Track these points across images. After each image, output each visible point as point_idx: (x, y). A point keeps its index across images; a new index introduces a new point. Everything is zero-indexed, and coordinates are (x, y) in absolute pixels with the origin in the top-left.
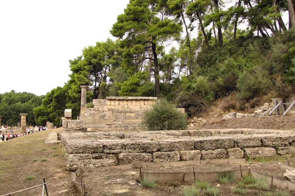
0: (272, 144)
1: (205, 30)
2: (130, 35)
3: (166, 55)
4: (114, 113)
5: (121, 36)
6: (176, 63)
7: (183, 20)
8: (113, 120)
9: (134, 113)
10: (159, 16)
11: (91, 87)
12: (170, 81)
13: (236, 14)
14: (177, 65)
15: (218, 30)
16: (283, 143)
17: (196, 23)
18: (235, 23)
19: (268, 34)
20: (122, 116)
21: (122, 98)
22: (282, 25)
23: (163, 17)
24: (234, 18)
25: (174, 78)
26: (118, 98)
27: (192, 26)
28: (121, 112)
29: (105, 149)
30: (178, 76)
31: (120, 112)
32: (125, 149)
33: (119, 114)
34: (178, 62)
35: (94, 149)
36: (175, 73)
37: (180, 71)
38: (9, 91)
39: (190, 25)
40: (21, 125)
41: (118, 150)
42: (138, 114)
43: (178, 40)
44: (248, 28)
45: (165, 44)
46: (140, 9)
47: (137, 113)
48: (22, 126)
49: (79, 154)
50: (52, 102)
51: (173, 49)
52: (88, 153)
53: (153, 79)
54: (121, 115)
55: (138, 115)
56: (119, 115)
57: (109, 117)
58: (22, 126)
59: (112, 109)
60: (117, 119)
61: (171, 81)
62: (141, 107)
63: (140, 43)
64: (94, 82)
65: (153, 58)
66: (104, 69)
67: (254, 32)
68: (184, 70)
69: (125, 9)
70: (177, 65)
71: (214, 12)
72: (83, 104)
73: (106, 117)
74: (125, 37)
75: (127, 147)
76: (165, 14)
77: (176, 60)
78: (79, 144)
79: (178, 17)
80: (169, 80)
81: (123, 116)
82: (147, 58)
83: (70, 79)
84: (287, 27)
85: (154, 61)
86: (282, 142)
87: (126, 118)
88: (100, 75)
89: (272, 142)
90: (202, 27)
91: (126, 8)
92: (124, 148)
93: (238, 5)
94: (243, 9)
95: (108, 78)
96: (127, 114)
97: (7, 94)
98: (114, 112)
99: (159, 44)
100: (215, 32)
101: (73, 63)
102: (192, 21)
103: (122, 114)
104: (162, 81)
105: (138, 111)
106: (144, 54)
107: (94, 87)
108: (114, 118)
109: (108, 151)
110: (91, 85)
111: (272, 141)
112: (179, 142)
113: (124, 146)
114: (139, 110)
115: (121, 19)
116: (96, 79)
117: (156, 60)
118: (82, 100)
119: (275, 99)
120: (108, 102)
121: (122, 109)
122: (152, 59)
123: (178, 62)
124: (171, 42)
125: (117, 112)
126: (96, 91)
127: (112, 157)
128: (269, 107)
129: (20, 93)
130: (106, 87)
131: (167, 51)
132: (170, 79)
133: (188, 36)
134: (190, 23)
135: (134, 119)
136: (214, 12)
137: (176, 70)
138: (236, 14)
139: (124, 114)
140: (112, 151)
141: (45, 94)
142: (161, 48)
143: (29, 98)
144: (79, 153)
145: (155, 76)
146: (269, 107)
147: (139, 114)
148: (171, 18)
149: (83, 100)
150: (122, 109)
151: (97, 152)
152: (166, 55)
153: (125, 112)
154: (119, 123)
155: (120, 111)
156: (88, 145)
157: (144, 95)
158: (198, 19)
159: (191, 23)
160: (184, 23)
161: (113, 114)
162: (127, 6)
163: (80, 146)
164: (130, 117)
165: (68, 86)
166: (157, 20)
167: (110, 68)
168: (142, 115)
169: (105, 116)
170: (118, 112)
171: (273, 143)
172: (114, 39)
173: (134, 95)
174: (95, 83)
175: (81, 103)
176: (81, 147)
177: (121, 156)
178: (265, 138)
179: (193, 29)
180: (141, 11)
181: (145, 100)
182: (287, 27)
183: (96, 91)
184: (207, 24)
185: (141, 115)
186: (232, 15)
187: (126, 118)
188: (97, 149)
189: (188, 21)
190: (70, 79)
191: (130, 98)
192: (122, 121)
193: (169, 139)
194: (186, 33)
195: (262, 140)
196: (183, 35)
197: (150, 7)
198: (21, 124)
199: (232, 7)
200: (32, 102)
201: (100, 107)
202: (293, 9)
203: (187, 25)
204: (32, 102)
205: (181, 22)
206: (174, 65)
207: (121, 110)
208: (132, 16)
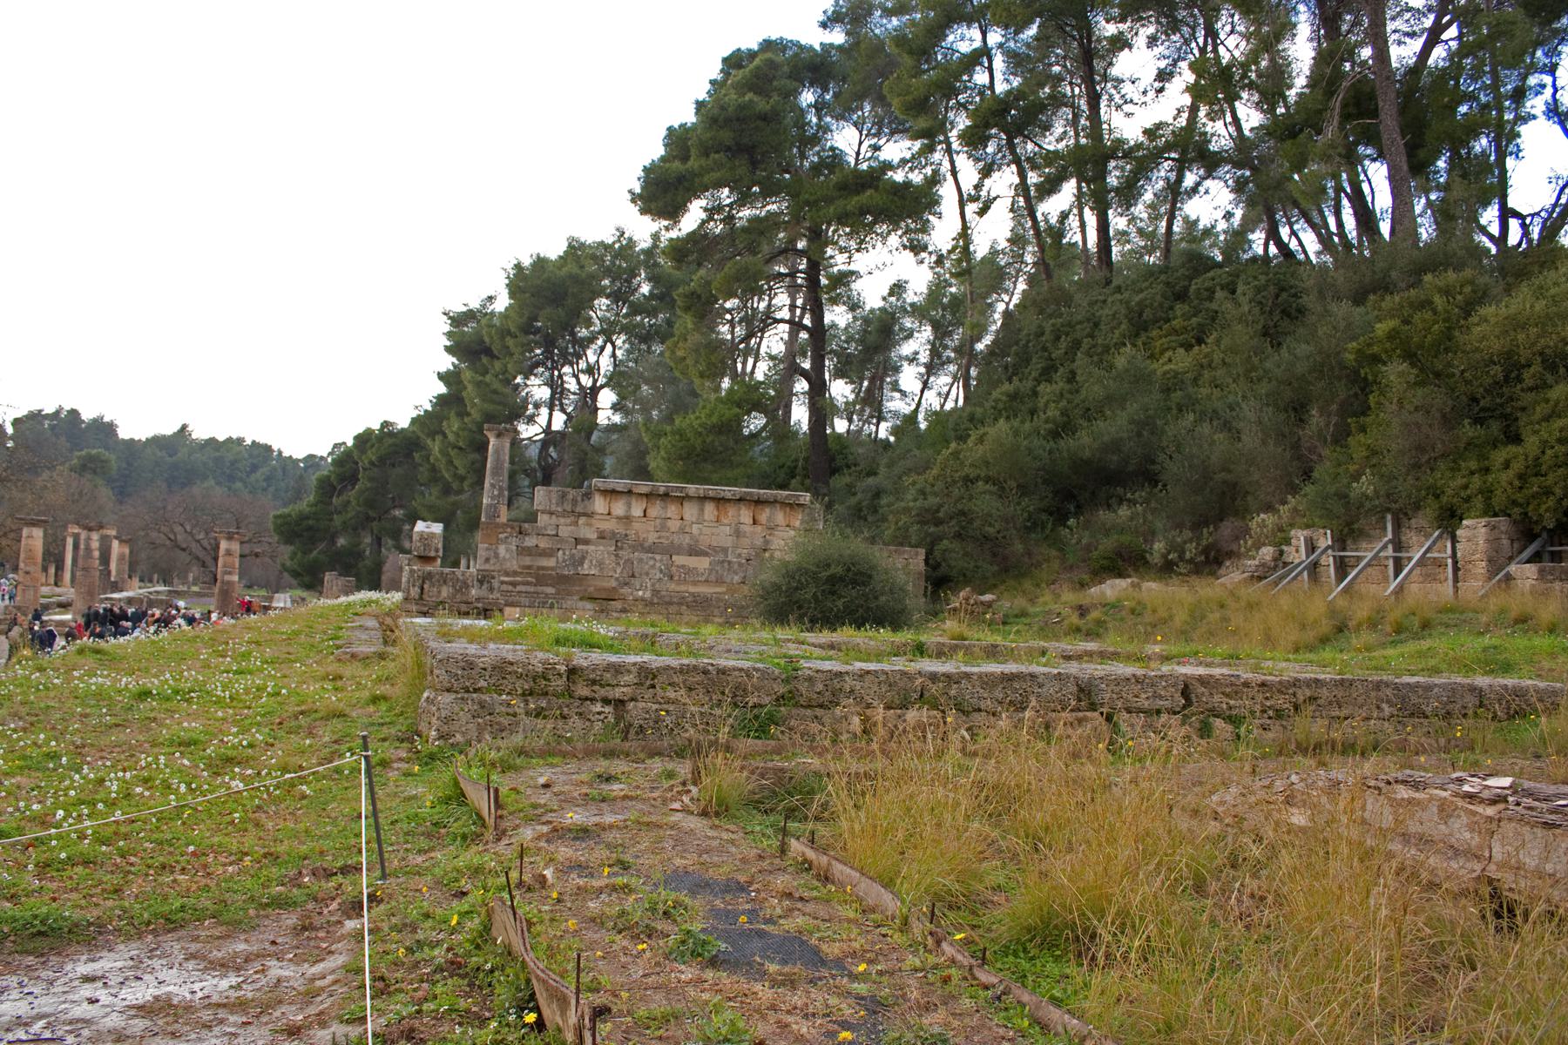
0: (1225, 706)
1: (1040, 217)
2: (711, 212)
3: (868, 308)
4: (621, 552)
5: (673, 212)
6: (907, 349)
7: (946, 165)
8: (617, 579)
9: (706, 554)
10: (846, 139)
11: (527, 431)
12: (877, 425)
13: (1173, 155)
14: (912, 359)
15: (1094, 218)
16: (1268, 704)
17: (1004, 182)
18: (1175, 193)
19: (1304, 251)
20: (653, 567)
21: (661, 487)
22: (1366, 218)
23: (860, 143)
24: (1165, 169)
25: (896, 414)
26: (643, 487)
27: (983, 193)
28: (652, 549)
29: (574, 682)
30: (913, 407)
31: (650, 550)
32: (653, 686)
33: (644, 556)
34: (919, 342)
35: (534, 680)
36: (904, 394)
37: (925, 386)
38: (169, 429)
39: (978, 187)
40: (216, 580)
41: (625, 690)
42: (723, 562)
43: (917, 248)
44: (1228, 216)
45: (861, 262)
46: (762, 105)
47: (721, 557)
48: (223, 582)
49: (475, 695)
50: (355, 484)
51: (898, 288)
52: (509, 694)
53: (800, 414)
54: (651, 563)
55: (726, 564)
56: (641, 560)
57: (600, 564)
58: (223, 582)
59: (614, 534)
60: (633, 576)
61: (884, 426)
62: (738, 533)
63: (833, 149)
64: (544, 411)
65: (807, 321)
66: (591, 356)
67: (1251, 237)
68: (942, 381)
69: (701, 99)
70: (912, 359)
71: (1083, 141)
72: (490, 506)
73: (586, 566)
74: (693, 216)
75: (661, 680)
76: (869, 131)
77: (910, 336)
78: (479, 657)
79: (930, 149)
80: (875, 421)
81: (658, 565)
82: (782, 321)
83: (441, 389)
84: (1385, 228)
85: (811, 335)
86: (1267, 698)
87: (671, 577)
88: (573, 380)
89: (1225, 700)
90: (1028, 199)
91: (702, 96)
92: (649, 682)
93: (1185, 115)
94: (1205, 139)
95: (607, 398)
96: (679, 560)
97: (156, 441)
98: (622, 548)
99: (840, 262)
100: (1083, 226)
101: (458, 320)
102: (986, 172)
103: (658, 557)
104: (841, 426)
105: (725, 550)
106: (771, 300)
107: (544, 431)
108: (619, 571)
109: (585, 692)
110: (531, 420)
111: (1227, 695)
112: (864, 674)
113: (647, 676)
114: (728, 542)
115: (677, 139)
116: (552, 397)
117: (819, 332)
118: (487, 485)
119: (1305, 532)
120: (599, 504)
121: (656, 535)
122: (805, 328)
123: (919, 342)
124: (888, 258)
125: (634, 549)
126: (551, 449)
127: (599, 713)
128: (1276, 566)
129: (212, 441)
130: (594, 437)
131: (872, 293)
132: (880, 419)
133: (965, 234)
134: (975, 181)
135: (707, 581)
136: (1083, 141)
137: (909, 378)
138: (1173, 155)
139: (666, 557)
140: (602, 692)
141: (323, 449)
142: (844, 278)
143: (255, 461)
144: (476, 691)
145: (811, 399)
146: (1276, 566)
147: (729, 562)
148: (896, 149)
149: (493, 486)
150: (656, 535)
151: (547, 694)
152: (868, 308)
153: (670, 551)
154: (640, 593)
155: (646, 545)
156: (512, 664)
157: (768, 481)
158: (1014, 167)
159: (982, 180)
160: (949, 175)
161: (617, 556)
162: (708, 86)
163: (482, 665)
164: (689, 571)
165: (427, 423)
166: (837, 156)
167: (619, 353)
168: (740, 565)
169: (581, 563)
170: (640, 546)
171: (1232, 702)
172: (643, 229)
173: (715, 477)
174: (547, 417)
175: (485, 501)
176: (485, 669)
177: (635, 711)
178: (1202, 680)
179: (989, 208)
180: (766, 114)
181: (759, 502)
182: (1385, 228)
183: (551, 449)
184: (1050, 187)
185: (736, 566)
186: (1155, 157)
187: (671, 577)
188: (545, 679)
189: (968, 172)
190: (441, 389)
191: (692, 489)
192: (653, 585)
193: (827, 662)
194: (959, 226)
195: (1186, 686)
196: (943, 233)
197: (808, 97)
198: (219, 577)
199: (1159, 126)
200: (265, 484)
201: (562, 520)
202: (1404, 159)
203: (964, 189)
204: (265, 480)
205: (936, 172)
206: (901, 358)
207: (652, 537)
208: (726, 136)
